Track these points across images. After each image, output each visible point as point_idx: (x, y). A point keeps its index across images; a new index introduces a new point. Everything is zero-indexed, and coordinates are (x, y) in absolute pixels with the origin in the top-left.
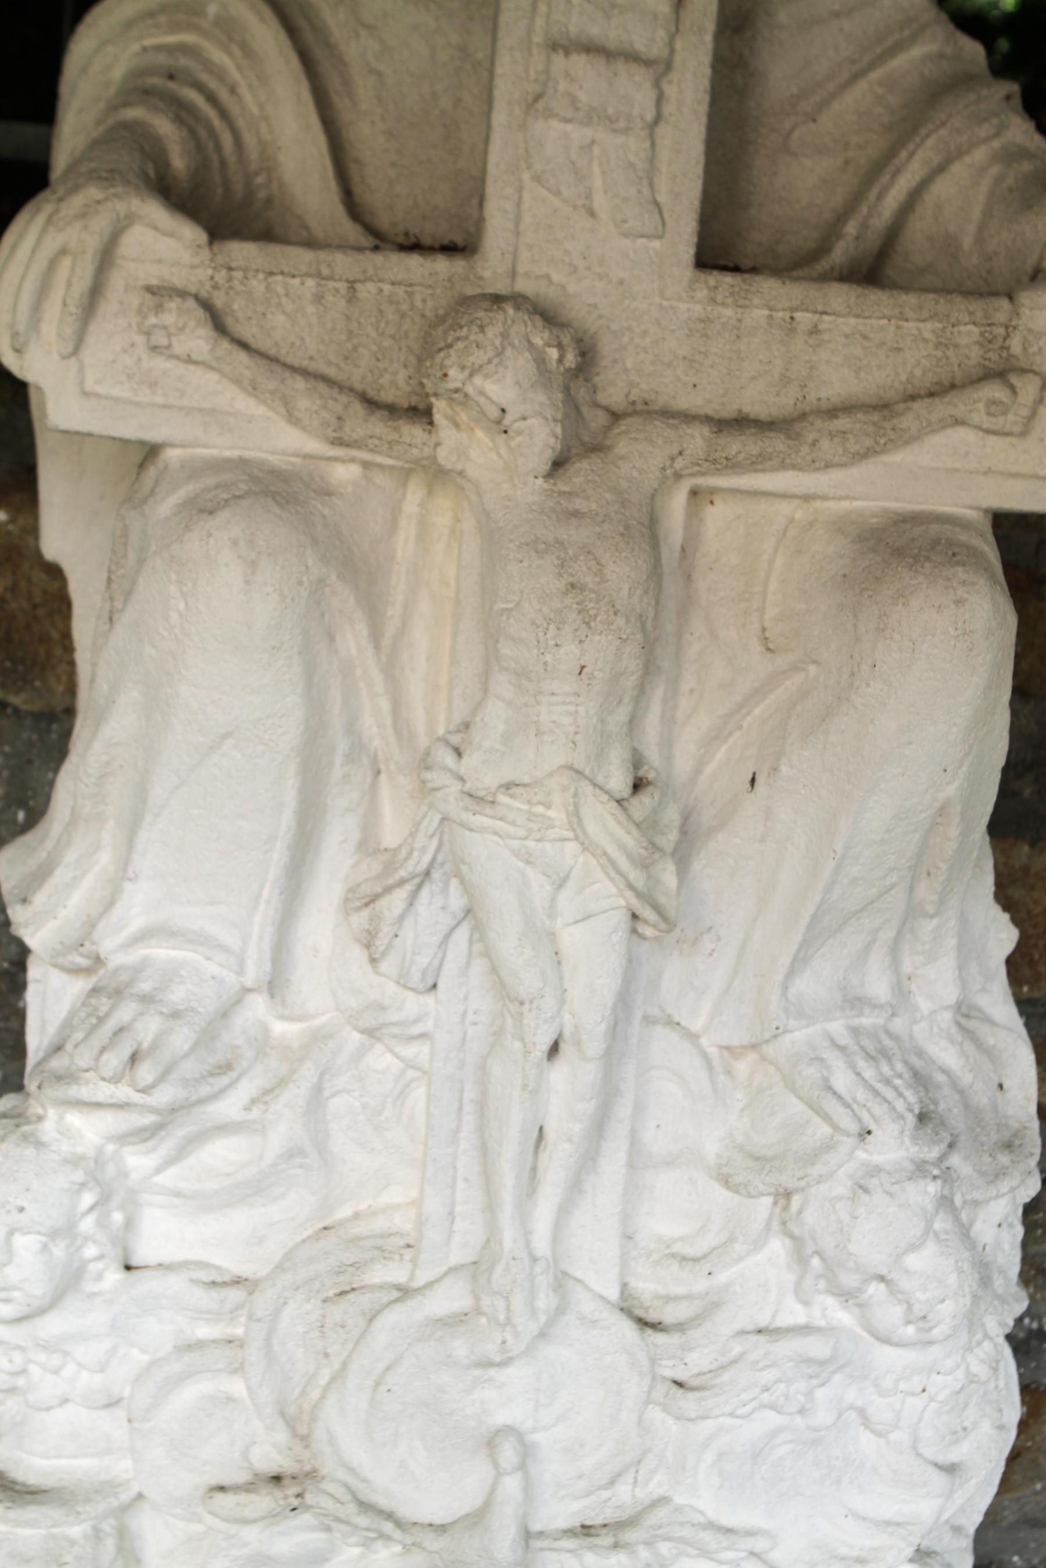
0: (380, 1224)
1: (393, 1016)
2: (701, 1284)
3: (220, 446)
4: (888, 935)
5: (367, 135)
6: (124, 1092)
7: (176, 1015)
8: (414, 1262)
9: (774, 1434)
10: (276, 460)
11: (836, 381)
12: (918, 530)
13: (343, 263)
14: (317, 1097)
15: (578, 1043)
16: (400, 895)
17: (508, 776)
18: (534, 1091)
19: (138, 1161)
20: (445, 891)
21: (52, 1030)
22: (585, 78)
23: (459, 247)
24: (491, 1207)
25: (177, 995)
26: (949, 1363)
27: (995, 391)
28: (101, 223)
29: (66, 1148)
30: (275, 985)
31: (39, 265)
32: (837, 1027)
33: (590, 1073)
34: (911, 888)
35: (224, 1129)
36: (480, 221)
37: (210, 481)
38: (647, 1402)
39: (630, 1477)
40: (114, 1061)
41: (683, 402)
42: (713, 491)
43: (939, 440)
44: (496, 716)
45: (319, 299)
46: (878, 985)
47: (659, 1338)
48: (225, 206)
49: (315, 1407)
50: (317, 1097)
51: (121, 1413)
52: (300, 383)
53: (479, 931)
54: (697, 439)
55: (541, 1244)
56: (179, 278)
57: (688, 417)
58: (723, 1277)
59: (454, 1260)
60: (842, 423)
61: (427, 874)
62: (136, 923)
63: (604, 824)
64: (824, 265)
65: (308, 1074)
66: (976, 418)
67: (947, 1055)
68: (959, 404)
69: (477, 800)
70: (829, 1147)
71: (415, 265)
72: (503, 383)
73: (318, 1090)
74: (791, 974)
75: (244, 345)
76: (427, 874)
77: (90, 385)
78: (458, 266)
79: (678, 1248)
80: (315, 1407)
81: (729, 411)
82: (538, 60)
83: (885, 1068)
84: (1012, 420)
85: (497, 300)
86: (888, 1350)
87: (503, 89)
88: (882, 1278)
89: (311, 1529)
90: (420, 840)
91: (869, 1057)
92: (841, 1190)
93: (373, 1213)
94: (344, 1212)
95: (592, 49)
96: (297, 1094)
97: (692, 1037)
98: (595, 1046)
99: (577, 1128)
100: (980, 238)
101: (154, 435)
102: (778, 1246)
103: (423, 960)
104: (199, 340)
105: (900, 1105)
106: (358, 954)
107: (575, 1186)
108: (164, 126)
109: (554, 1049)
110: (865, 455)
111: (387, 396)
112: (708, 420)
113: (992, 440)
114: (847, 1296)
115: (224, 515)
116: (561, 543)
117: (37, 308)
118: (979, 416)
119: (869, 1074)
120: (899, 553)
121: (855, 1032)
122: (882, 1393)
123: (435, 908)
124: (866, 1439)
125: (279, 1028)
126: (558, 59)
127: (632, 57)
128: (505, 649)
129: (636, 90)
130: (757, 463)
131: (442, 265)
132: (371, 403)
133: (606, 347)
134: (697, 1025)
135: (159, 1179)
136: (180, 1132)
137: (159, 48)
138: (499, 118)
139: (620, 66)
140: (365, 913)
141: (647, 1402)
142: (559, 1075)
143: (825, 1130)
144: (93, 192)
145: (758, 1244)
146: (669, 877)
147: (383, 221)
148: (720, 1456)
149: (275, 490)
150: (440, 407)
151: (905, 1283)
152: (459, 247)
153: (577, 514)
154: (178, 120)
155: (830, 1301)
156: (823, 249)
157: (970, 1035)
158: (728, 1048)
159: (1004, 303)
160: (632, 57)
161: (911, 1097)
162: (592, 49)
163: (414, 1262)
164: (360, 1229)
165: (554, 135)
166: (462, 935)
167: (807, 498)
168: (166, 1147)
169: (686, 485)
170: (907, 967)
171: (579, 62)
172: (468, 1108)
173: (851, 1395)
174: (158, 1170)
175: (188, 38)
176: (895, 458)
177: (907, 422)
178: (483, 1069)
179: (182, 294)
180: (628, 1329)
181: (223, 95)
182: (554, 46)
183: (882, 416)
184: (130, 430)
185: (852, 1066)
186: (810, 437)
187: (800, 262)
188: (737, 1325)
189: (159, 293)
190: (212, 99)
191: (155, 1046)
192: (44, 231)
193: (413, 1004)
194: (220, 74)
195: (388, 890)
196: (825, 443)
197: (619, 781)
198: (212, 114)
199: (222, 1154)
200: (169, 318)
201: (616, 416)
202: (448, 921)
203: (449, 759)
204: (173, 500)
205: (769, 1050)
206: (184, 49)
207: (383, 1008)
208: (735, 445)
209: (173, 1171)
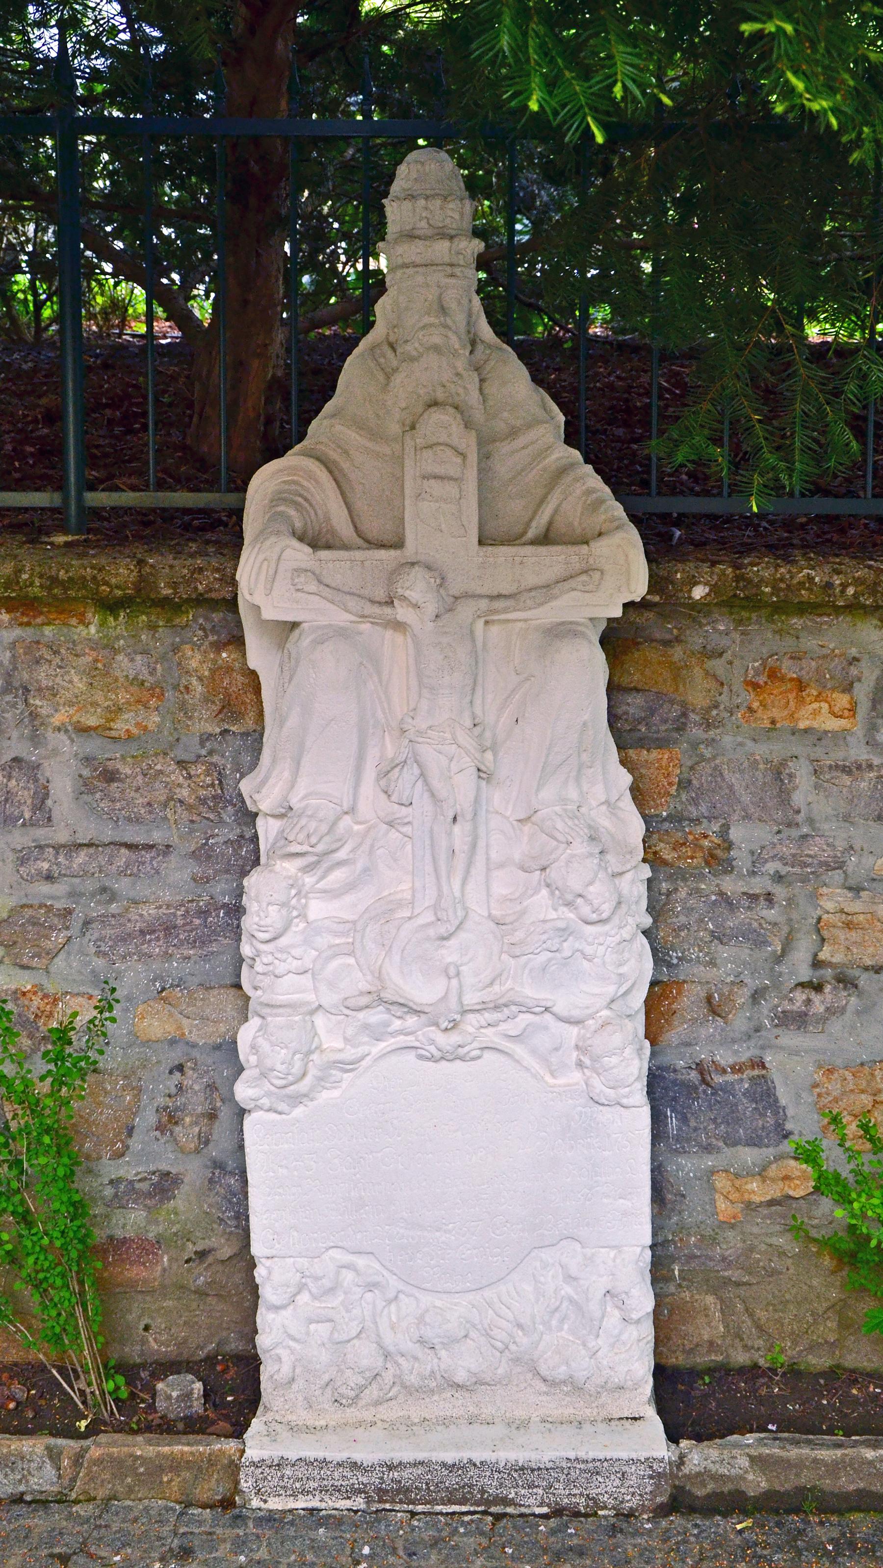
0: (399, 896)
1: (397, 816)
2: (519, 908)
3: (323, 621)
4: (573, 774)
5: (360, 505)
6: (305, 848)
7: (321, 821)
8: (413, 908)
9: (550, 960)
10: (342, 624)
11: (532, 580)
12: (562, 628)
13: (358, 555)
14: (371, 851)
15: (463, 816)
16: (397, 770)
17: (430, 723)
18: (450, 834)
19: (309, 880)
20: (412, 768)
21: (271, 840)
22: (434, 486)
23: (398, 544)
24: (438, 878)
25: (321, 814)
26: (613, 932)
27: (584, 577)
28: (277, 549)
29: (285, 873)
30: (351, 811)
31: (257, 565)
32: (557, 809)
33: (468, 826)
34: (579, 756)
35: (340, 864)
36: (403, 534)
37: (320, 633)
38: (502, 952)
39: (498, 982)
40: (301, 837)
41: (478, 592)
42: (493, 621)
43: (566, 597)
44: (424, 705)
45: (351, 568)
46: (573, 793)
47: (503, 927)
48: (318, 540)
49: (381, 967)
50: (371, 851)
51: (309, 975)
52: (348, 597)
53: (426, 783)
54: (484, 604)
55: (457, 894)
56: (303, 565)
57: (480, 596)
58: (525, 904)
59: (427, 905)
60: (533, 594)
61: (405, 762)
62: (302, 793)
63: (463, 738)
64: (524, 539)
65: (368, 841)
66: (579, 587)
67: (605, 822)
68: (572, 583)
69: (419, 733)
70: (556, 848)
71: (383, 554)
72: (417, 587)
73: (372, 846)
74: (538, 790)
75: (328, 586)
76: (405, 762)
77: (275, 604)
78: (398, 552)
79: (509, 897)
80: (381, 967)
81: (496, 593)
82: (419, 481)
83: (576, 822)
84: (590, 587)
85: (413, 564)
86: (589, 927)
87: (407, 492)
88: (580, 896)
89: (381, 1012)
90: (403, 749)
91: (570, 818)
92: (563, 864)
93: (395, 893)
94: (386, 893)
95: (436, 477)
96: (365, 847)
97: (507, 818)
98: (469, 816)
99: (466, 848)
100: (580, 524)
101: (297, 619)
102: (544, 892)
103: (406, 794)
104: (313, 587)
105: (582, 833)
106: (383, 796)
107: (467, 872)
108: (292, 512)
109: (455, 819)
110: (541, 604)
111: (377, 599)
112: (488, 596)
113: (587, 595)
114: (568, 904)
115: (327, 644)
116: (440, 643)
117: (257, 579)
118: (580, 587)
119: (570, 823)
120: (556, 636)
121: (565, 810)
122: (589, 944)
123: (410, 773)
124: (585, 963)
125: (356, 827)
126: (425, 481)
127: (450, 478)
128: (425, 680)
129: (451, 489)
130: (506, 610)
131: (392, 553)
132: (373, 602)
133: (450, 576)
134: (508, 814)
135: (318, 886)
136: (324, 866)
137: (284, 482)
138: (407, 502)
139: (446, 481)
140: (385, 779)
141: (502, 952)
142: (457, 829)
143: (555, 843)
144: (273, 539)
145: (536, 891)
146: (489, 755)
147: (370, 536)
148: (531, 970)
149: (342, 633)
150: (396, 602)
151: (589, 897)
152: (398, 544)
153: (446, 633)
154: (297, 510)
155: (565, 909)
156: (525, 533)
157: (615, 815)
158: (519, 821)
159: (585, 547)
160: (450, 478)
161: (586, 831)
162: (436, 477)
163: (413, 908)
164: (392, 898)
165: (426, 506)
166: (420, 783)
167: (526, 620)
168: (319, 872)
169: (483, 620)
170: (585, 789)
171: (432, 481)
172: (428, 847)
173: (577, 945)
174: (317, 882)
175: (295, 478)
176: (554, 603)
177: (556, 591)
178: (431, 831)
179: (306, 571)
180: (492, 925)
181: (309, 497)
182: (424, 477)
183: (546, 590)
184: (290, 618)
185: (563, 821)
186: (523, 599)
187: (512, 540)
188: (531, 920)
189: (298, 571)
190: (306, 500)
191: (315, 831)
192: (258, 553)
193: (404, 811)
194: (307, 490)
195: (393, 768)
196: (528, 601)
197: (468, 723)
198: (307, 505)
199: (338, 876)
200: (302, 579)
201: (456, 598)
202: (414, 778)
203: (410, 720)
204: (308, 641)
205: (533, 819)
206: (294, 482)
207: (394, 814)
208: (500, 604)
209: (322, 883)
